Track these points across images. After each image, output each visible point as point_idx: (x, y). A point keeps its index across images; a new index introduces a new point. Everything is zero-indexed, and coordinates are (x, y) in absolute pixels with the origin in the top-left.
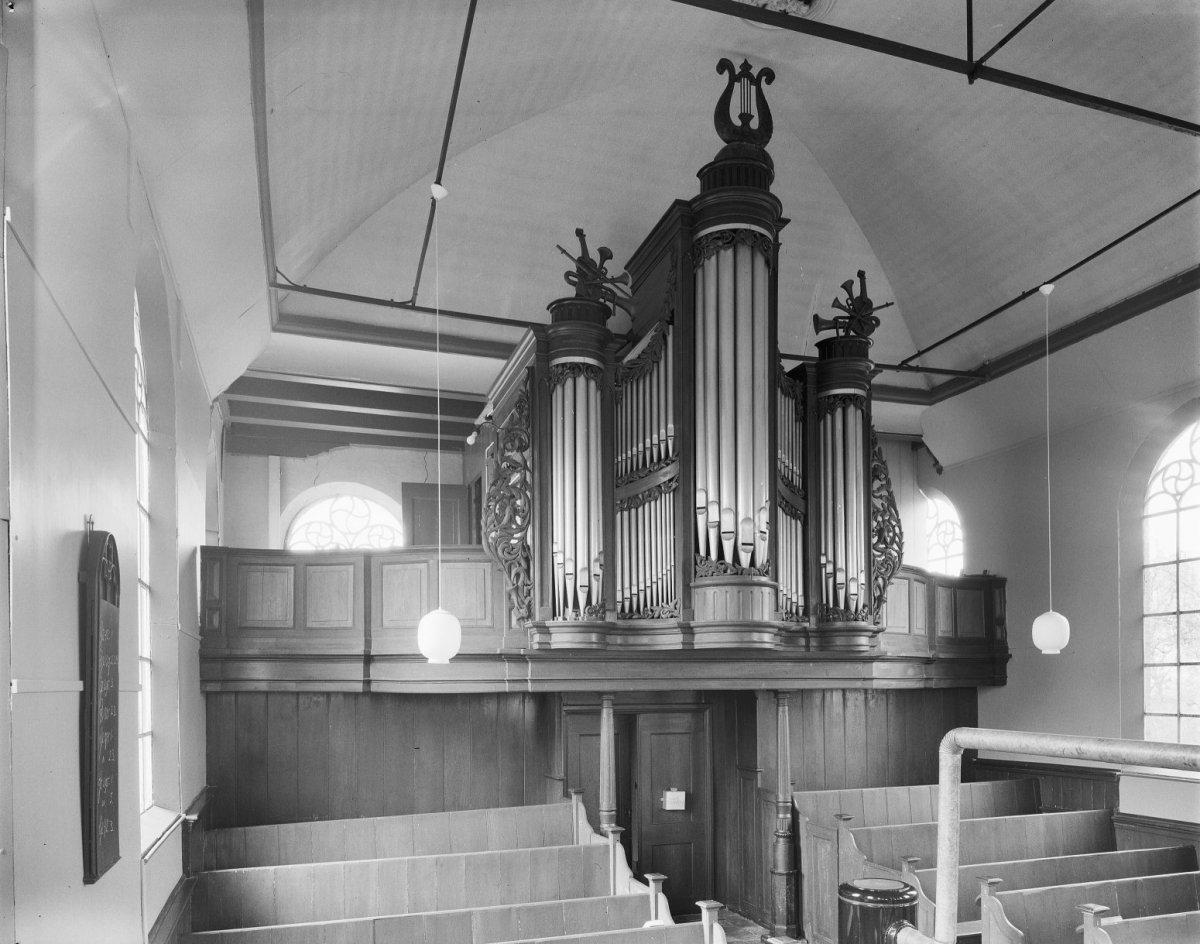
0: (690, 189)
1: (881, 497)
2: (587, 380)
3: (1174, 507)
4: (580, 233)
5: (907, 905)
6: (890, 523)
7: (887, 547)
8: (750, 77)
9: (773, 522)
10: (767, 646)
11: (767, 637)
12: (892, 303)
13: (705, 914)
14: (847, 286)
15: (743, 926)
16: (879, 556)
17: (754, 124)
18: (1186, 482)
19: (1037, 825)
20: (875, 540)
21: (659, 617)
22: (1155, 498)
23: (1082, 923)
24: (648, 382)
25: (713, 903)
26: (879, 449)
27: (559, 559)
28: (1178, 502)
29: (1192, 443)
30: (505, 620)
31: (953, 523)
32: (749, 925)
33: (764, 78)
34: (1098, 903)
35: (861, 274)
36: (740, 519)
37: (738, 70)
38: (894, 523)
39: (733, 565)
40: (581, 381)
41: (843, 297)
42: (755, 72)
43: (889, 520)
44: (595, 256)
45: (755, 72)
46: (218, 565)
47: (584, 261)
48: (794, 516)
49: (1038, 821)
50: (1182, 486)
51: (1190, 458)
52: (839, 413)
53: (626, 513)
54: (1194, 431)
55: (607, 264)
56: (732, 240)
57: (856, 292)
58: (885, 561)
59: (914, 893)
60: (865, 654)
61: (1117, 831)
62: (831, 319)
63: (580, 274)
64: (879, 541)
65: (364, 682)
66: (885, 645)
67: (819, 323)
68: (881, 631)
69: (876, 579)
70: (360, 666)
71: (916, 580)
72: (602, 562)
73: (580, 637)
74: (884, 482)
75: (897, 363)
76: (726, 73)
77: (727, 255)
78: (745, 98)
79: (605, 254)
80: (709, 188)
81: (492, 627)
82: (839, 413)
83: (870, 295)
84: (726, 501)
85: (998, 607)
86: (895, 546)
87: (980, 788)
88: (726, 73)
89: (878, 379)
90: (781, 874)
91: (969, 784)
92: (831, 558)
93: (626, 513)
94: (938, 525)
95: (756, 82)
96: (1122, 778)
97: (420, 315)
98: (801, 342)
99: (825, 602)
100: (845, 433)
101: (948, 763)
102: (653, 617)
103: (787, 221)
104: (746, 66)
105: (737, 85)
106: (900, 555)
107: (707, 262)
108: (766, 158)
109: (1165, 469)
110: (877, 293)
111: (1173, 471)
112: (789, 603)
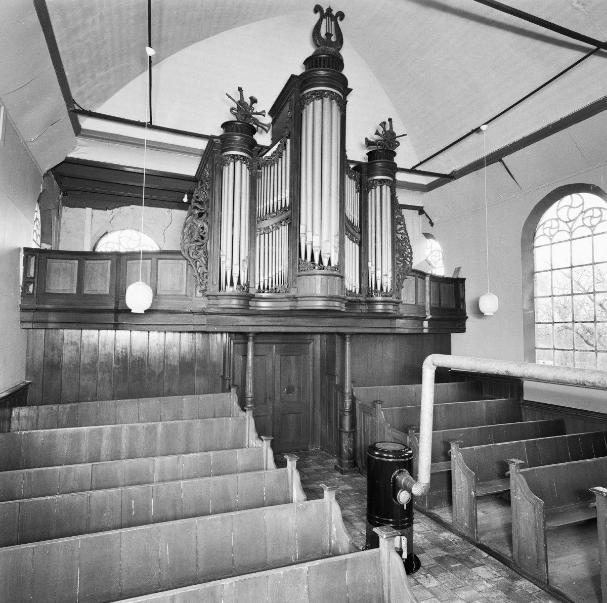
0: (299, 70)
2: (242, 163)
3: (549, 242)
4: (240, 89)
5: (407, 459)
6: (406, 247)
9: (342, 243)
12: (406, 135)
13: (289, 463)
15: (327, 459)
16: (400, 264)
17: (333, 39)
18: (560, 223)
19: (482, 405)
20: (397, 256)
21: (279, 292)
22: (540, 238)
23: (509, 470)
25: (310, 446)
28: (571, 236)
29: (558, 210)
30: (194, 290)
31: (439, 251)
32: (331, 458)
34: (520, 459)
35: (390, 120)
36: (323, 240)
38: (408, 247)
39: (319, 265)
41: (381, 131)
42: (334, 13)
43: (405, 246)
44: (248, 101)
45: (334, 13)
46: (34, 257)
47: (241, 103)
49: (483, 403)
50: (553, 231)
51: (557, 217)
52: (378, 188)
53: (266, 235)
54: (559, 204)
55: (254, 105)
56: (320, 95)
57: (388, 129)
59: (411, 452)
61: (523, 410)
63: (239, 109)
66: (402, 310)
67: (369, 143)
68: (401, 302)
69: (398, 275)
71: (419, 277)
75: (409, 168)
77: (318, 103)
78: (328, 26)
79: (254, 101)
80: (309, 69)
81: (186, 296)
82: (378, 188)
83: (394, 130)
84: (317, 231)
85: (461, 293)
86: (408, 259)
87: (448, 387)
89: (400, 177)
90: (346, 432)
91: (446, 384)
93: (262, 236)
94: (432, 252)
95: (334, 19)
96: (524, 381)
98: (357, 153)
99: (370, 286)
100: (380, 198)
101: (428, 374)
102: (276, 292)
103: (351, 90)
104: (329, 10)
105: (324, 21)
107: (307, 107)
108: (340, 54)
109: (544, 224)
110: (398, 131)
111: (548, 224)
112: (351, 286)
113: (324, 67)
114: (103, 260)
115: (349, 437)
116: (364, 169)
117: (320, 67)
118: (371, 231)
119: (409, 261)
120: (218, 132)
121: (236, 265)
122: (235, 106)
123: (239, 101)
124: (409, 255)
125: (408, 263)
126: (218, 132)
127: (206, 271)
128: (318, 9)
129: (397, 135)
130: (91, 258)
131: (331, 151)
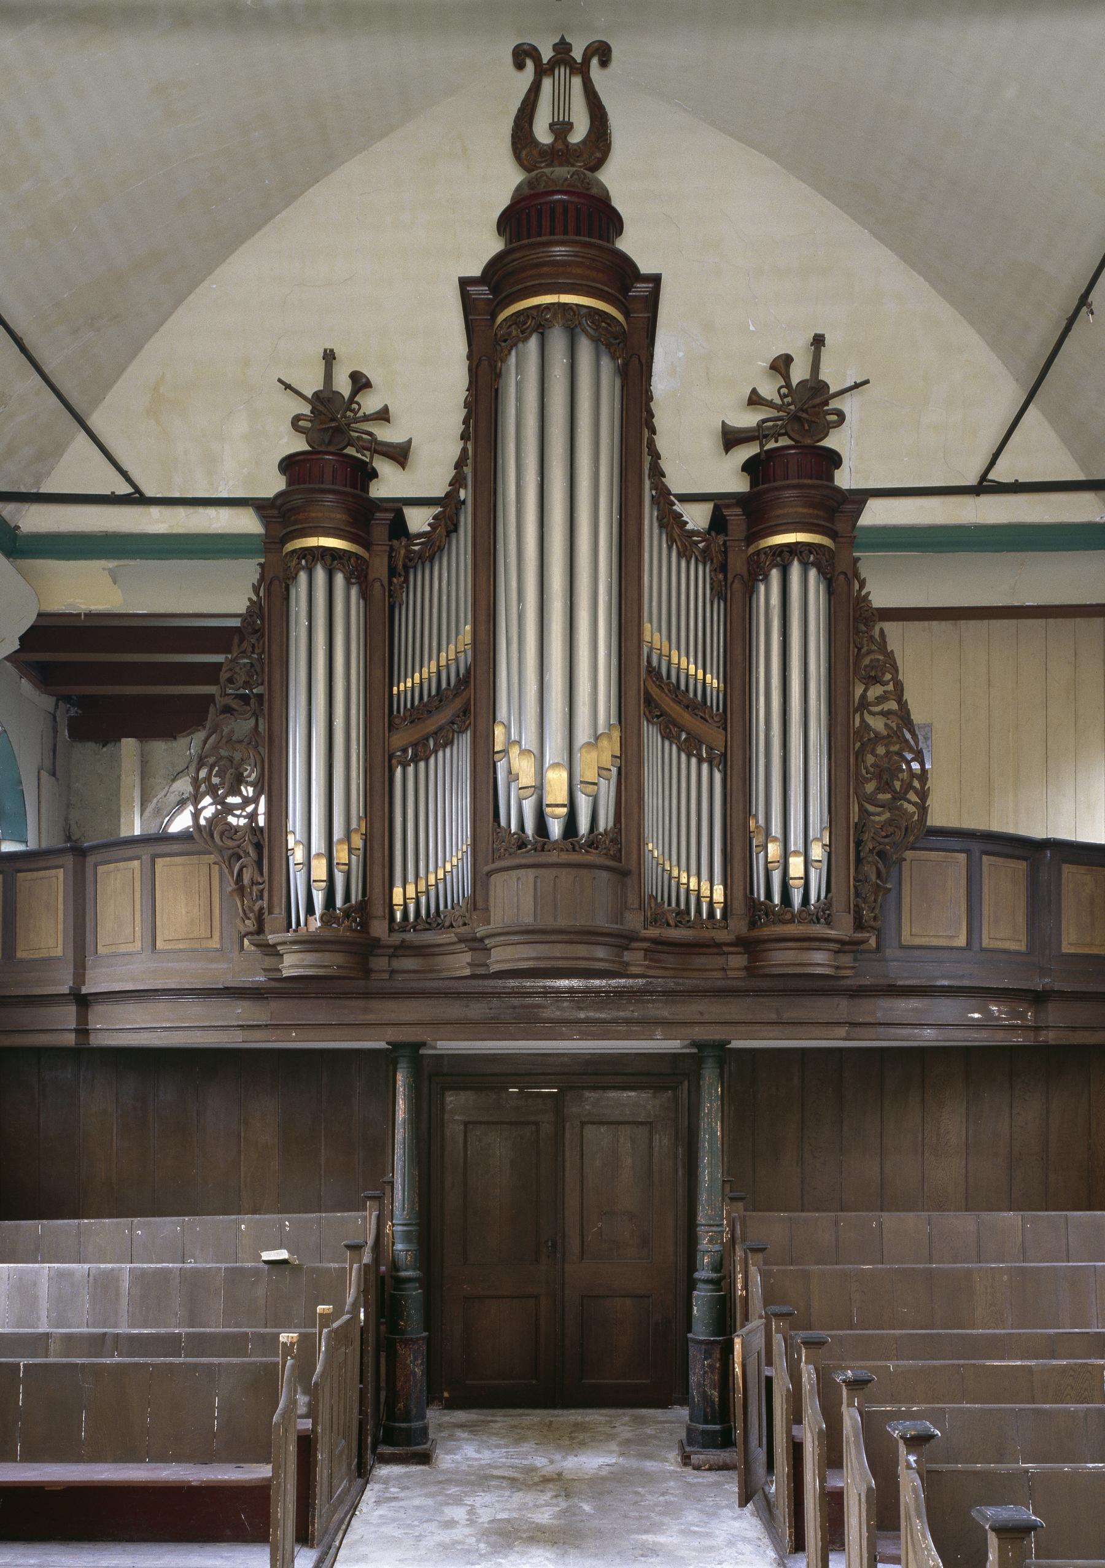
1: (884, 714)
7: (894, 798)
8: (570, 63)
10: (819, 971)
11: (819, 957)
14: (781, 365)
16: (878, 814)
24: (445, 563)
26: (882, 631)
27: (298, 855)
33: (595, 62)
37: (547, 54)
40: (320, 574)
41: (769, 390)
42: (577, 54)
44: (343, 386)
45: (577, 54)
48: (691, 746)
58: (890, 822)
60: (848, 982)
62: (755, 425)
64: (879, 790)
65: (76, 1031)
67: (731, 439)
70: (72, 1009)
72: (827, 841)
73: (309, 958)
74: (890, 687)
76: (530, 65)
78: (561, 100)
83: (823, 376)
86: (912, 796)
88: (530, 65)
92: (761, 822)
95: (582, 70)
97: (155, 511)
104: (563, 48)
105: (547, 83)
106: (923, 810)
110: (833, 376)
113: (565, 233)
114: (931, 850)
115: (708, 1355)
116: (734, 515)
117: (552, 233)
118: (648, 736)
119: (914, 804)
120: (273, 484)
121: (318, 855)
122: (306, 409)
123: (316, 395)
124: (916, 784)
125: (911, 808)
126: (273, 484)
127: (260, 880)
128: (522, 55)
129: (833, 390)
130: (32, 866)
131: (504, 533)
